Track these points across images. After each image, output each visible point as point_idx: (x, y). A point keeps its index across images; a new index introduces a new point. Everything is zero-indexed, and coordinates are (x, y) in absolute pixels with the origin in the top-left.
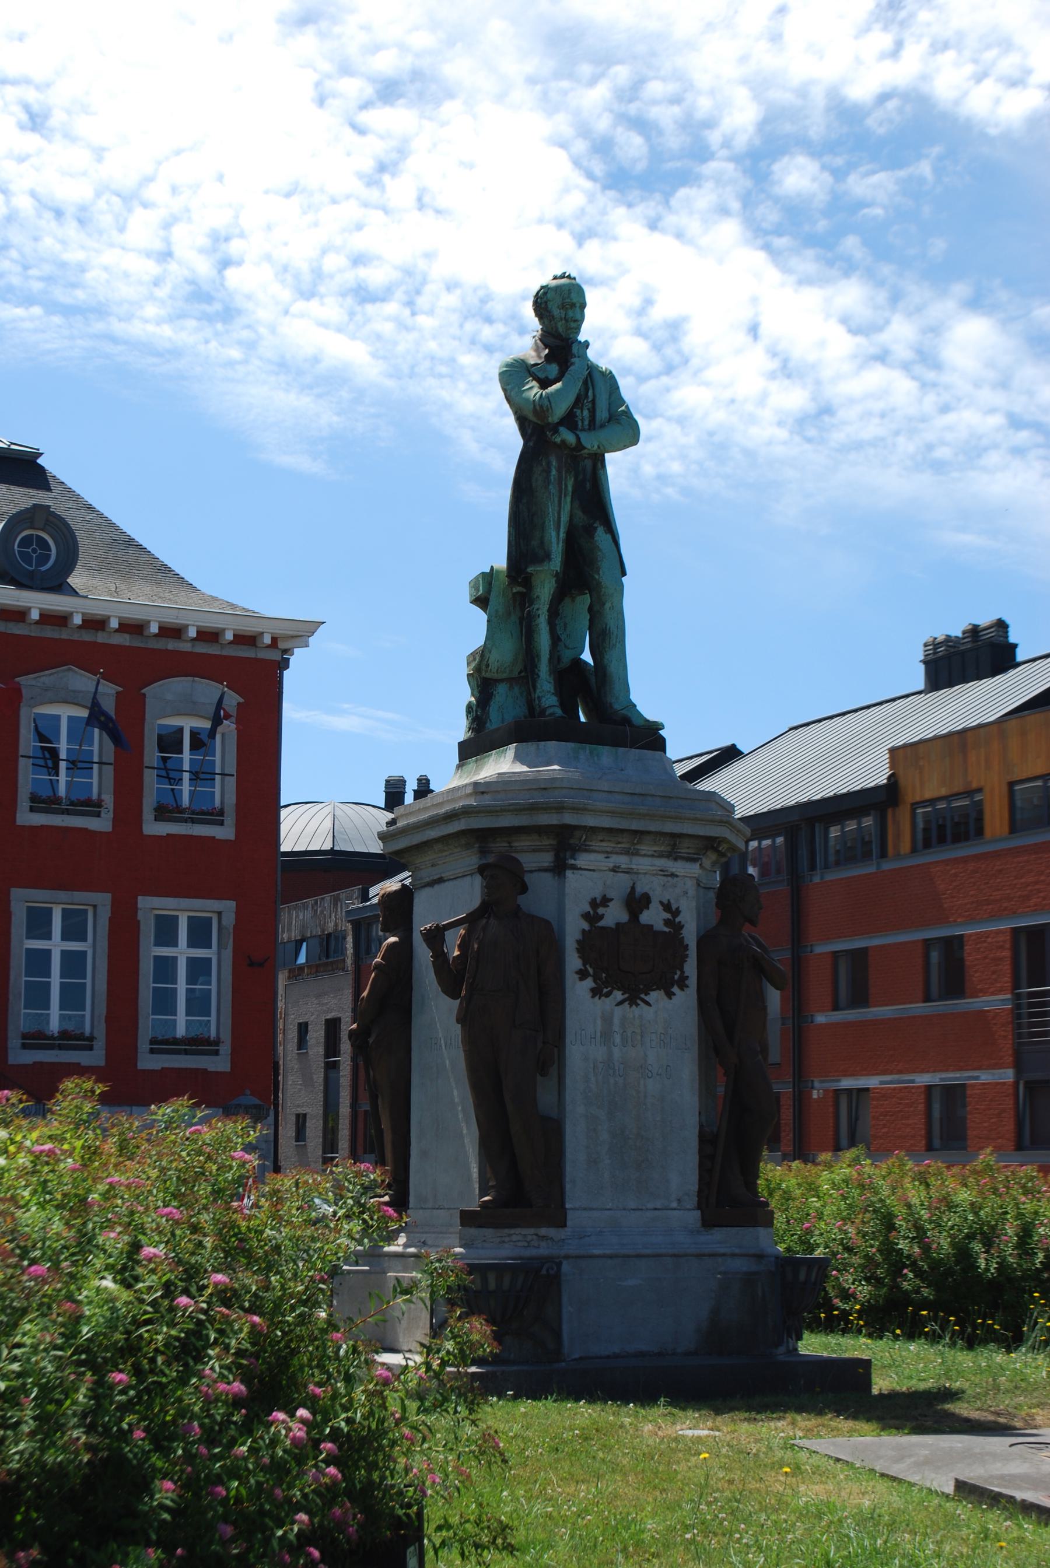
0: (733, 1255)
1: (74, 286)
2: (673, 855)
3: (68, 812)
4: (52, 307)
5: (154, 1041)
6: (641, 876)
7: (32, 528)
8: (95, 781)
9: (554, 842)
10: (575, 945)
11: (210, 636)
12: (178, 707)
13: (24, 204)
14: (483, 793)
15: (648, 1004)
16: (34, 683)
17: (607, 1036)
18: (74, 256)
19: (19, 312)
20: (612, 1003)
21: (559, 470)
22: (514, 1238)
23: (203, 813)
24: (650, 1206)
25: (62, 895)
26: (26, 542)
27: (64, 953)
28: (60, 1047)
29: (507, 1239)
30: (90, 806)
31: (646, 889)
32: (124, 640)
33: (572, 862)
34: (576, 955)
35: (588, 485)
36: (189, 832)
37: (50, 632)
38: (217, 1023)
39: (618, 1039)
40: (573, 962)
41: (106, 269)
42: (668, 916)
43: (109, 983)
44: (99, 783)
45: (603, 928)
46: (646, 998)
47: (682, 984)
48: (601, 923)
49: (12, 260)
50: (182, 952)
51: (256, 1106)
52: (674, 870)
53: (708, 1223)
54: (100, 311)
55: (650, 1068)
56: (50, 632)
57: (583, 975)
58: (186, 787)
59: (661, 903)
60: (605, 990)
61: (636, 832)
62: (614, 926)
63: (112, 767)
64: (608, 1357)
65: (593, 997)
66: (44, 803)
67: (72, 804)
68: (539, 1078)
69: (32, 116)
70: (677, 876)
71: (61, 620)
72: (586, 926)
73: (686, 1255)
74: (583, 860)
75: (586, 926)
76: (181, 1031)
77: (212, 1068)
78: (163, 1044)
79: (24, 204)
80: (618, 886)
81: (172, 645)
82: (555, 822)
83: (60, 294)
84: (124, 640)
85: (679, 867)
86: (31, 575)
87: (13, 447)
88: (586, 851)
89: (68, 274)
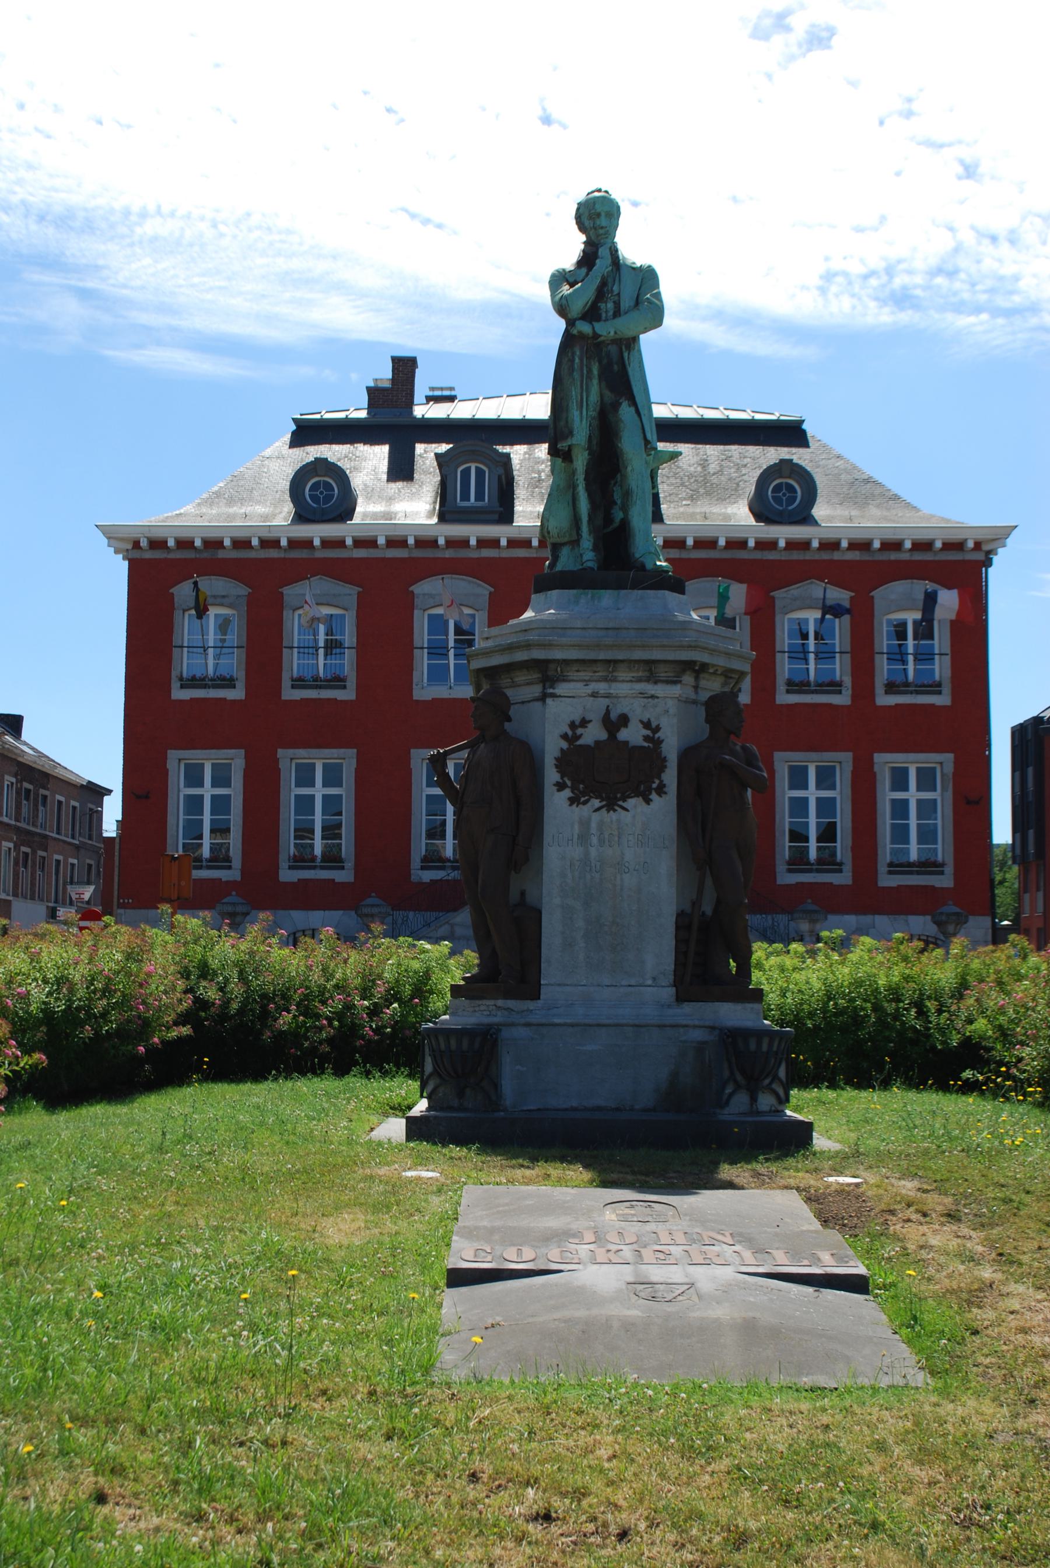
0: (695, 1027)
1: (1011, 293)
2: (652, 678)
4: (996, 312)
5: (891, 865)
7: (781, 477)
8: (838, 666)
9: (540, 675)
10: (554, 762)
11: (923, 546)
12: (897, 605)
13: (968, 238)
14: (487, 638)
15: (626, 810)
16: (785, 595)
17: (584, 838)
18: (1007, 270)
19: (972, 319)
20: (590, 810)
21: (581, 360)
22: (482, 1008)
23: (924, 686)
24: (624, 983)
25: (813, 755)
26: (778, 489)
27: (818, 799)
28: (818, 871)
30: (834, 687)
31: (625, 711)
33: (551, 691)
35: (616, 367)
37: (796, 556)
38: (943, 849)
39: (595, 840)
40: (551, 775)
41: (1034, 276)
42: (648, 732)
43: (853, 821)
44: (840, 668)
45: (580, 746)
46: (624, 805)
47: (661, 790)
48: (580, 742)
49: (963, 281)
50: (913, 795)
51: (957, 914)
53: (681, 998)
54: (1034, 308)
56: (796, 556)
57: (560, 786)
58: (911, 667)
59: (641, 722)
60: (583, 799)
61: (609, 662)
62: (592, 745)
63: (849, 655)
64: (566, 1110)
65: (570, 805)
66: (796, 686)
67: (916, 686)
69: (967, 168)
71: (805, 545)
72: (565, 745)
74: (561, 689)
75: (565, 745)
76: (914, 856)
77: (938, 885)
78: (898, 867)
79: (968, 238)
80: (595, 709)
81: (893, 556)
82: (526, 658)
83: (1001, 302)
84: (855, 556)
85: (659, 690)
86: (781, 513)
87: (782, 418)
88: (564, 681)
89: (1005, 284)
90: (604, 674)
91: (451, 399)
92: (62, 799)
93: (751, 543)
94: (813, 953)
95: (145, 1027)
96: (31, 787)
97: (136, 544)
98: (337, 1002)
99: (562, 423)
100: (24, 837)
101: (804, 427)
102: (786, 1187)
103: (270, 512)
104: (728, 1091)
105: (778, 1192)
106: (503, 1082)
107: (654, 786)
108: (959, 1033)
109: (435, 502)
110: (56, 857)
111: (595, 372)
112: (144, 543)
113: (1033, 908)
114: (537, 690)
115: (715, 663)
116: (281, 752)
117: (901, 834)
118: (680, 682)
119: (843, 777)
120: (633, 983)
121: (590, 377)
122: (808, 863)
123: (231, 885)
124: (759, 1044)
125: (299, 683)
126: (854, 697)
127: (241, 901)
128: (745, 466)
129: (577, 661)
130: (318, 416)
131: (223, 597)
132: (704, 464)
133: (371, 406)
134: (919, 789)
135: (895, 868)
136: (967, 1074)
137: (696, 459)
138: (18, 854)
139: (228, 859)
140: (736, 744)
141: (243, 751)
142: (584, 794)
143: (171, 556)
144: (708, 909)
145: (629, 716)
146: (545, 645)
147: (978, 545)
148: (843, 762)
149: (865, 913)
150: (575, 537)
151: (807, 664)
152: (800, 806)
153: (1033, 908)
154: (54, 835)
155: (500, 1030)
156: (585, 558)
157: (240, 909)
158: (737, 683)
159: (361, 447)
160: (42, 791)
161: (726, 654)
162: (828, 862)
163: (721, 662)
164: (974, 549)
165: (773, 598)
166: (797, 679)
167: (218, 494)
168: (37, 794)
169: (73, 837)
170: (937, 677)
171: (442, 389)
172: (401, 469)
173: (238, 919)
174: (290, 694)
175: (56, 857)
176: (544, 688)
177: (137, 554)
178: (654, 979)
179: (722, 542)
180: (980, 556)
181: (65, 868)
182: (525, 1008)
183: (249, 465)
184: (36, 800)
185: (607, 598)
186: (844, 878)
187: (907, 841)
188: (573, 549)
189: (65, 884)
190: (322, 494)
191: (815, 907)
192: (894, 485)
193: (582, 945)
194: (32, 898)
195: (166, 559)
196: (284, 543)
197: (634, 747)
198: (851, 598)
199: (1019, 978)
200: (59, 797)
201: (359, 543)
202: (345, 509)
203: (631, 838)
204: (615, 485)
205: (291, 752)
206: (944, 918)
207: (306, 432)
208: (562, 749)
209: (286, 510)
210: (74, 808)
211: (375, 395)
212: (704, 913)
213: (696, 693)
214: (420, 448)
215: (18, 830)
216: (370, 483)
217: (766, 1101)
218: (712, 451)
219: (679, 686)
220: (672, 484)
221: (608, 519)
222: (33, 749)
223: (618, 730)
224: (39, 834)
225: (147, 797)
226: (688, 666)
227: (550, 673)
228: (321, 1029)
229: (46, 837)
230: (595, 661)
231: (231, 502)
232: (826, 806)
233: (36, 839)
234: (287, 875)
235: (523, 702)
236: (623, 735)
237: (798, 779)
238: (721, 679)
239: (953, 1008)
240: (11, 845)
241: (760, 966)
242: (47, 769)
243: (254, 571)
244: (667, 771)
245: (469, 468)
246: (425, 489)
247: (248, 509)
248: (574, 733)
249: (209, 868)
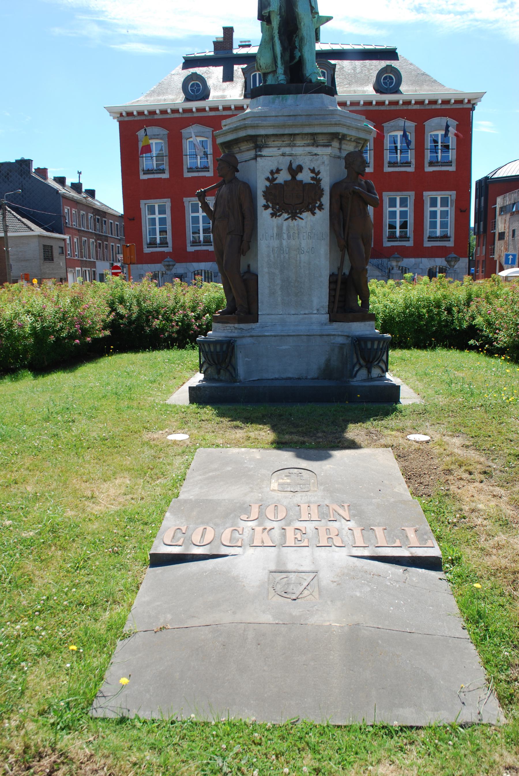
0: (339, 335)
2: (315, 144)
3: (400, 166)
5: (429, 237)
6: (298, 157)
7: (387, 73)
8: (409, 155)
9: (253, 145)
10: (262, 193)
11: (446, 102)
12: (435, 129)
17: (279, 235)
22: (228, 328)
23: (445, 163)
24: (302, 312)
25: (399, 193)
26: (385, 78)
28: (400, 241)
29: (225, 328)
30: (407, 164)
31: (301, 163)
32: (418, 107)
33: (260, 153)
34: (263, 198)
36: (440, 169)
37: (393, 108)
38: (450, 231)
39: (285, 236)
40: (261, 201)
42: (314, 175)
44: (410, 156)
45: (276, 184)
46: (301, 216)
47: (321, 207)
50: (439, 209)
51: (455, 257)
52: (316, 152)
53: (332, 320)
55: (303, 249)
56: (393, 108)
57: (266, 207)
59: (310, 169)
60: (278, 214)
61: (291, 135)
62: (283, 183)
65: (272, 217)
66: (392, 164)
67: (402, 163)
68: (242, 255)
70: (318, 155)
71: (396, 103)
73: (313, 335)
74: (265, 152)
75: (268, 184)
76: (438, 234)
77: (407, 245)
78: (431, 238)
81: (433, 107)
84: (418, 107)
88: (267, 147)
90: (288, 142)
91: (249, 46)
92: (112, 221)
93: (374, 103)
94: (399, 284)
95: (85, 332)
96: (99, 217)
97: (121, 115)
98: (180, 315)
100: (98, 237)
101: (397, 51)
102: (386, 446)
103: (174, 98)
104: (356, 369)
105: (381, 450)
106: (238, 368)
107: (317, 205)
108: (467, 322)
109: (242, 90)
110: (112, 244)
112: (124, 114)
113: (481, 252)
114: (252, 154)
115: (350, 134)
116: (185, 199)
117: (433, 225)
118: (331, 145)
119: (411, 202)
120: (307, 312)
122: (396, 238)
123: (168, 253)
124: (373, 344)
125: (190, 170)
126: (416, 168)
127: (171, 260)
128: (372, 69)
129: (273, 135)
130: (193, 55)
131: (158, 135)
132: (354, 69)
133: (215, 49)
134: (441, 206)
135: (431, 238)
136: (471, 342)
137: (351, 67)
138: (97, 244)
139: (167, 243)
140: (362, 181)
141: (170, 199)
142: (279, 211)
143: (136, 119)
144: (346, 271)
145: (303, 166)
146: (255, 127)
147: (469, 101)
148: (411, 196)
149: (418, 257)
150: (274, 69)
151: (397, 154)
152: (393, 214)
153: (481, 252)
154: (110, 236)
155: (236, 341)
156: (280, 79)
157: (171, 263)
158: (363, 147)
159: (211, 68)
160: (104, 219)
161: (357, 128)
162: (404, 237)
163: (353, 133)
164: (467, 103)
165: (383, 126)
166: (392, 161)
167: (153, 92)
168: (102, 220)
169: (118, 236)
170: (450, 159)
171: (245, 42)
172: (228, 77)
173: (171, 267)
174: (187, 175)
175: (112, 244)
176: (256, 152)
177: (122, 119)
178: (318, 310)
179: (362, 103)
180: (470, 106)
181: (116, 248)
182: (250, 327)
183: (166, 78)
184: (102, 222)
185: (290, 99)
186: (410, 244)
187: (435, 227)
188: (274, 75)
189: (116, 254)
190: (195, 89)
191: (398, 256)
192: (435, 76)
193: (280, 293)
194: (104, 260)
195: (134, 120)
196: (181, 111)
197: (306, 184)
198: (416, 125)
199: (497, 297)
200: (110, 221)
201: (212, 109)
202: (205, 95)
203: (305, 234)
204: (296, 37)
205: (189, 199)
206: (450, 259)
207: (190, 62)
208: (266, 186)
209: (181, 96)
210: (117, 225)
211: (217, 45)
212: (344, 273)
213: (340, 152)
214: (236, 67)
215: (95, 234)
216: (215, 83)
217: (376, 372)
218: (358, 63)
219: (330, 148)
220: (341, 78)
221: (292, 57)
222: (100, 202)
223: (297, 174)
224: (104, 236)
225: (134, 220)
226: (335, 136)
227: (258, 143)
228: (173, 326)
229: (107, 236)
230: (283, 135)
231: (159, 94)
232: (403, 214)
233: (103, 237)
234: (190, 249)
235: (246, 161)
236: (300, 177)
237: (393, 203)
238: (354, 144)
239: (465, 310)
240: (94, 240)
241: (373, 292)
242: (105, 210)
243: (172, 123)
244: (324, 196)
245: (256, 74)
246: (238, 84)
247: (166, 97)
248: (273, 177)
249: (160, 247)
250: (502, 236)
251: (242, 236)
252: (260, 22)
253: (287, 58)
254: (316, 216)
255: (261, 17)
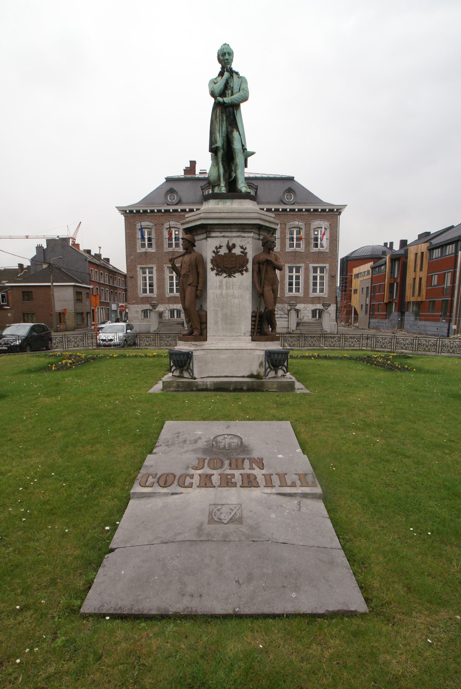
39: (224, 287)
40: (209, 266)
42: (242, 250)
47: (247, 270)
57: (212, 269)
75: (214, 255)
80: (224, 242)
99: (213, 139)
111: (225, 119)
121: (222, 121)
147: (337, 210)
193: (221, 323)
211: (186, 171)
215: (109, 286)
221: (230, 176)
236: (234, 251)
250: (356, 291)
251: (197, 287)
252: (210, 153)
253: (227, 176)
254: (244, 276)
255: (211, 150)
